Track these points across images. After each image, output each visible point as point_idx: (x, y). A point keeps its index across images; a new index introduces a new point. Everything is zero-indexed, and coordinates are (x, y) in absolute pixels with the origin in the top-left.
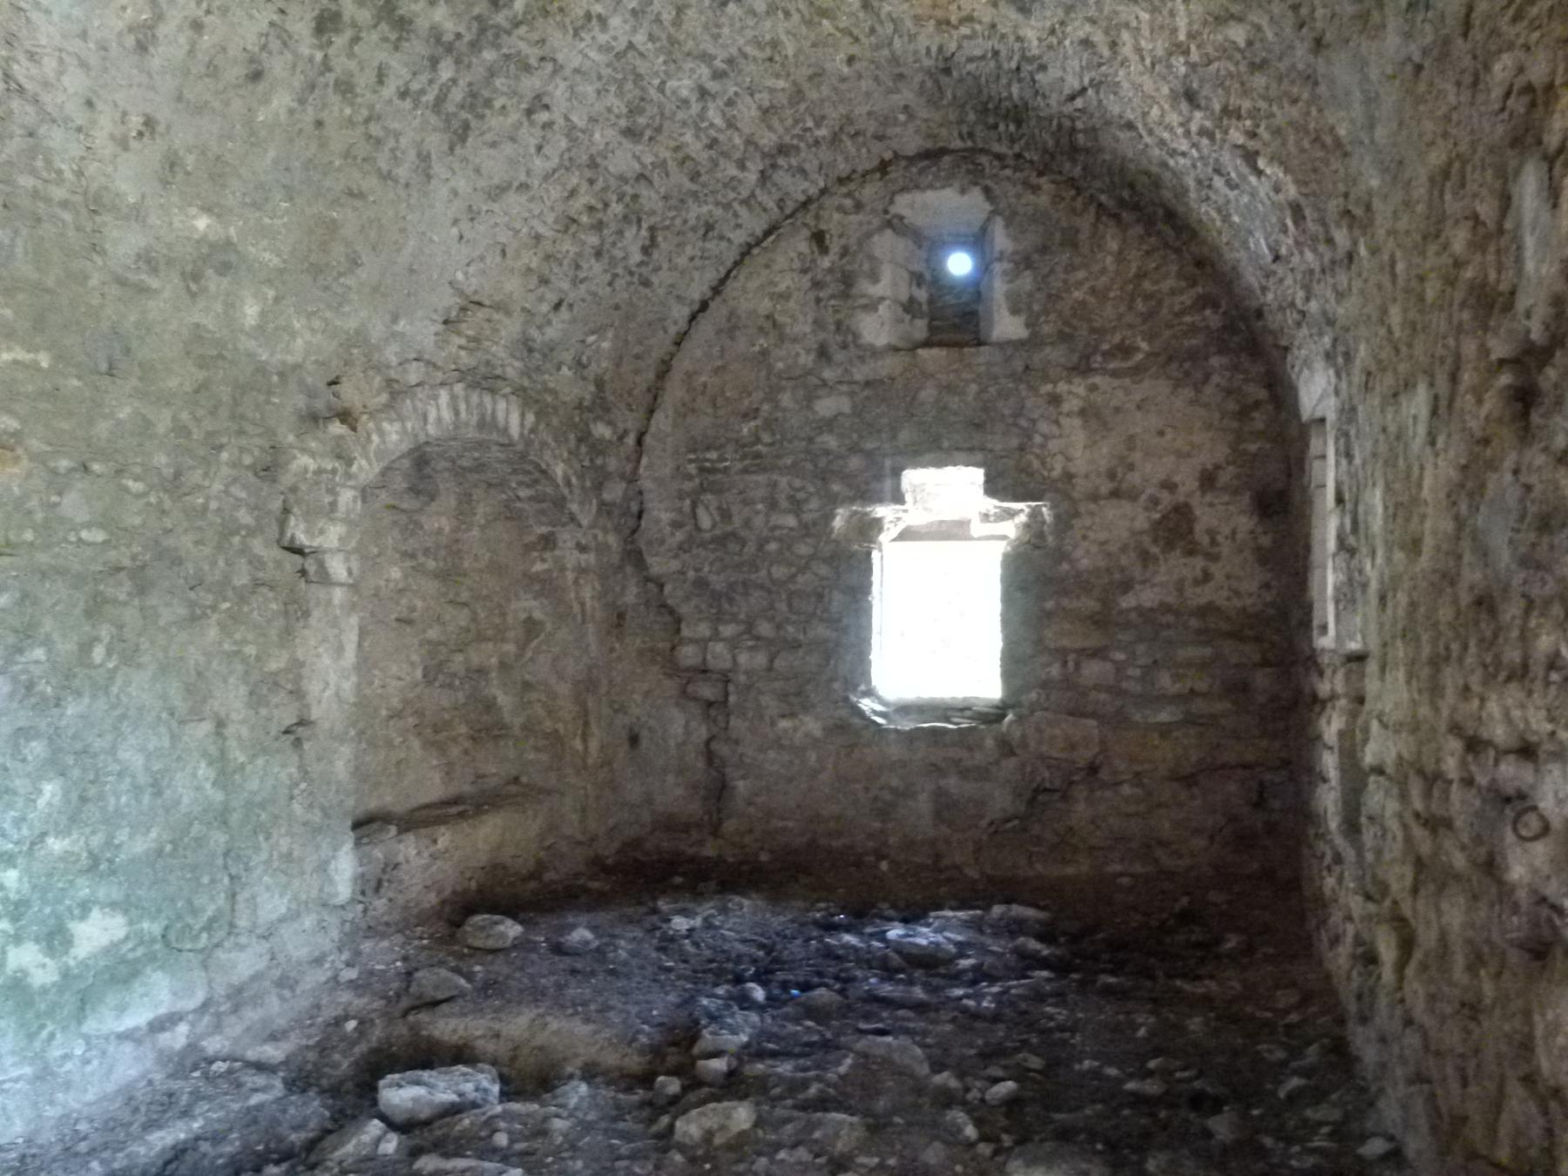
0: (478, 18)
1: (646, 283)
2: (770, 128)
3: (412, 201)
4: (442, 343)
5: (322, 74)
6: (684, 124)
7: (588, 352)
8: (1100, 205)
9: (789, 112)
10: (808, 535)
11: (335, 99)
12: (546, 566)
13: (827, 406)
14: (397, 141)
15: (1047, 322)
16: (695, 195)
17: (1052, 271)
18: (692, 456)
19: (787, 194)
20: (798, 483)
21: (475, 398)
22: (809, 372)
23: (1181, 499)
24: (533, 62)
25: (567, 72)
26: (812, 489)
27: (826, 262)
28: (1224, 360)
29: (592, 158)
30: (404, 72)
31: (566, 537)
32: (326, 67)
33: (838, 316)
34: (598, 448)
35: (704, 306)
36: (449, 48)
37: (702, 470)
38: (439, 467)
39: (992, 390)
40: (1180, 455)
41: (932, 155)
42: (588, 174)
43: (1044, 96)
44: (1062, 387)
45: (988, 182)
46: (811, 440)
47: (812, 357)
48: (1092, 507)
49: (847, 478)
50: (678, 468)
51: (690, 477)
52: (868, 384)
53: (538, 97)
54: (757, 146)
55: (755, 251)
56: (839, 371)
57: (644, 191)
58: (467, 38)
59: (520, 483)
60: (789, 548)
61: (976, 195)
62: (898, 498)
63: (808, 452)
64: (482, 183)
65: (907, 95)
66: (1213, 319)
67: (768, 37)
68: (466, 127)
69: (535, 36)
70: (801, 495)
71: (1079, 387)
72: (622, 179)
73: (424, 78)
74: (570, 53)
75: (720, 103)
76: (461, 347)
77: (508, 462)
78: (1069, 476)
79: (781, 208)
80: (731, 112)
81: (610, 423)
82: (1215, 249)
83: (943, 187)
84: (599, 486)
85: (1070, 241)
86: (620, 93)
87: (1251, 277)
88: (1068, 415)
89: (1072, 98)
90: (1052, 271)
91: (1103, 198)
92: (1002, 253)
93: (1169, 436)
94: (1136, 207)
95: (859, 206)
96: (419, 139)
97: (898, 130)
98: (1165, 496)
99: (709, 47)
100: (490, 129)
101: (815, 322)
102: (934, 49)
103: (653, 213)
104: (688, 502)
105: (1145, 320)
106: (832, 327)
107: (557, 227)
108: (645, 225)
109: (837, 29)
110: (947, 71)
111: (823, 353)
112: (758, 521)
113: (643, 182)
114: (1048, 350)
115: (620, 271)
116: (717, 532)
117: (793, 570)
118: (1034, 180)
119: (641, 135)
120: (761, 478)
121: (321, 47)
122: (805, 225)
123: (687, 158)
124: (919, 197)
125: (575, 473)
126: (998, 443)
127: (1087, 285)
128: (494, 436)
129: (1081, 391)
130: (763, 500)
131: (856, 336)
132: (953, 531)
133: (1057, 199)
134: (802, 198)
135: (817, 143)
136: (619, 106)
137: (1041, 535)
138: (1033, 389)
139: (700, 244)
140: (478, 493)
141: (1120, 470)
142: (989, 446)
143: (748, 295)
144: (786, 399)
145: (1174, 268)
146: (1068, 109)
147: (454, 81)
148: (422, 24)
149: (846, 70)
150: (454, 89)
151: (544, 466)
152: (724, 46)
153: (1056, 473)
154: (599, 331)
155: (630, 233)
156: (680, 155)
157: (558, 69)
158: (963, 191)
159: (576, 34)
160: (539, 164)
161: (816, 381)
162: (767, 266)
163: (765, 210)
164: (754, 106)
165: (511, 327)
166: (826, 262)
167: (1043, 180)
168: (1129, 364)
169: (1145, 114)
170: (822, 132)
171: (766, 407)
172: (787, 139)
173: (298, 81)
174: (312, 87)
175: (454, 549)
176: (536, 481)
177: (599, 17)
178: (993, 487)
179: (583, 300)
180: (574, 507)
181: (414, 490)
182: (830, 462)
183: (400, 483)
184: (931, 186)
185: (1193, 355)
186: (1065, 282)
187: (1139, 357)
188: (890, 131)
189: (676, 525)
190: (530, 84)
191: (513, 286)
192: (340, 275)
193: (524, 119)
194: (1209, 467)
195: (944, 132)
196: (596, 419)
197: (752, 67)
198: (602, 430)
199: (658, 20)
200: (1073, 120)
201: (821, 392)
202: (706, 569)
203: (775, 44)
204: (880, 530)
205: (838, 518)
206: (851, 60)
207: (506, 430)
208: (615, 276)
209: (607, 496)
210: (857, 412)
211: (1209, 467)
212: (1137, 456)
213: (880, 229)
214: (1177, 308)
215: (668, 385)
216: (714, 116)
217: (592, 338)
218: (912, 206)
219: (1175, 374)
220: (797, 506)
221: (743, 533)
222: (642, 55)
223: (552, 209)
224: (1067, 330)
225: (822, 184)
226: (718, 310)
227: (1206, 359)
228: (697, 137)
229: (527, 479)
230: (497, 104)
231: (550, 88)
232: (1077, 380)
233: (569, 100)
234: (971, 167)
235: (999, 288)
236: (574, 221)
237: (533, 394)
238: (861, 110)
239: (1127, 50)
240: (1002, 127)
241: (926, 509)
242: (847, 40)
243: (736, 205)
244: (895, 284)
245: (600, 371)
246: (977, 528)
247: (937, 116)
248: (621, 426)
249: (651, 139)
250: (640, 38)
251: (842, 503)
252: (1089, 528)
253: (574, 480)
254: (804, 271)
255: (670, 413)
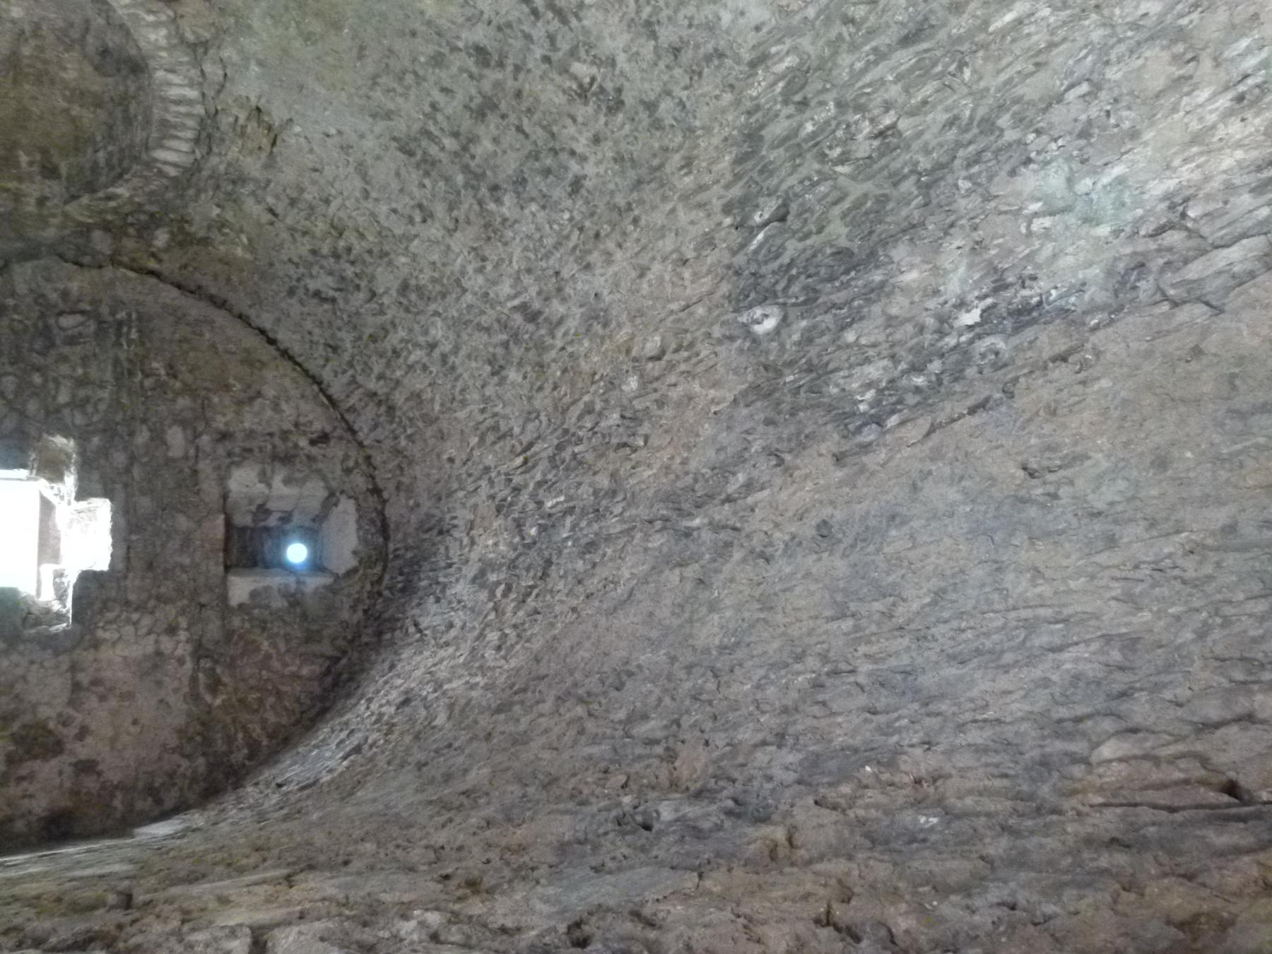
0: (484, 174)
1: (291, 292)
2: (407, 399)
3: (356, 99)
4: (242, 102)
5: (448, 43)
6: (411, 330)
7: (232, 235)
8: (339, 659)
9: (417, 414)
10: (48, 413)
11: (431, 49)
12: (24, 165)
13: (176, 438)
14: (401, 95)
15: (243, 620)
16: (360, 338)
17: (285, 623)
18: (134, 316)
19: (359, 415)
20: (102, 407)
21: (191, 123)
22: (207, 424)
23: (68, 746)
24: (455, 213)
25: (448, 240)
26: (95, 419)
27: (303, 443)
28: (202, 769)
29: (387, 254)
30: (449, 111)
31: (54, 188)
32: (455, 49)
33: (256, 450)
34: (145, 232)
35: (272, 342)
36: (465, 148)
37: (120, 324)
38: (129, 82)
39: (184, 577)
40: (113, 741)
41: (384, 529)
42: (376, 250)
43: (420, 604)
44: (183, 635)
45: (361, 572)
46: (144, 421)
47: (221, 426)
48: (65, 667)
49: (104, 452)
50: (123, 303)
51: (113, 313)
52: (195, 472)
53: (432, 216)
54: (394, 389)
55: (315, 387)
56: (208, 449)
57: (362, 296)
58: (473, 164)
59: (110, 154)
60: (35, 394)
61: (353, 563)
62: (82, 494)
63: (133, 418)
64: (369, 161)
65: (426, 504)
66: (239, 756)
67: (468, 397)
68: (411, 154)
69: (472, 217)
70: (90, 409)
71: (183, 650)
72: (372, 278)
73: (445, 125)
74: (460, 242)
75: (425, 360)
76: (237, 119)
77: (132, 146)
78: (96, 645)
79: (348, 410)
80: (418, 367)
81: (167, 249)
82: (296, 746)
83: (359, 537)
84: (106, 227)
85: (310, 638)
86: (434, 281)
87: (267, 774)
88: (157, 642)
89: (416, 625)
90: (285, 623)
91: (344, 661)
92: (304, 583)
93: (132, 729)
94: (335, 684)
95: (348, 471)
96: (403, 113)
97: (403, 501)
98: (73, 731)
99: (463, 353)
100: (409, 173)
101: (252, 431)
102: (455, 522)
103: (347, 302)
104: (88, 308)
105: (240, 701)
106: (247, 445)
107: (336, 220)
108: (337, 294)
109: (472, 449)
110: (441, 532)
111: (224, 436)
112: (64, 369)
113: (368, 295)
114: (218, 623)
115: (302, 270)
116: (55, 331)
117: (11, 397)
118: (361, 607)
119: (404, 296)
120: (108, 376)
121: (466, 47)
122: (335, 428)
123: (387, 332)
124: (352, 518)
125: (119, 207)
126: (133, 582)
127: (272, 651)
128: (155, 135)
129: (179, 652)
130: (85, 374)
131: (238, 464)
132: (48, 546)
133: (345, 625)
134: (356, 427)
135: (396, 438)
136: (424, 279)
137: (38, 622)
138: (183, 612)
139: (322, 341)
140: (102, 115)
141: (101, 689)
142: (131, 575)
143: (277, 379)
144: (184, 402)
145: (284, 721)
146: (409, 622)
147: (443, 149)
148: (481, 130)
149: (445, 457)
150: (436, 148)
151: (126, 177)
152: (463, 363)
153: (100, 634)
154: (251, 247)
155: (330, 280)
156: (389, 327)
157: (451, 232)
158: (355, 553)
159: (474, 249)
160: (383, 209)
161: (200, 429)
162: (303, 396)
163: (348, 396)
164: (422, 387)
165: (253, 166)
166: (303, 443)
167: (360, 614)
168: (202, 689)
169: (398, 676)
170: (403, 442)
171: (178, 385)
172: (398, 413)
173: (444, 23)
174: (439, 34)
175: (43, 78)
176: (111, 168)
177: (484, 267)
178: (88, 579)
179: (277, 235)
180: (85, 200)
181: (105, 52)
182: (122, 437)
183: (113, 40)
184: (360, 528)
185: (208, 742)
186: (277, 635)
187: (208, 698)
188: (402, 494)
189: (65, 294)
190: (439, 209)
191: (288, 175)
192: (298, 24)
193: (416, 202)
194: (100, 767)
195: (400, 536)
196: (172, 233)
197: (449, 386)
198: (161, 238)
199: (483, 313)
200: (401, 628)
201: (189, 432)
202: (16, 317)
203: (464, 403)
204: (51, 480)
205: (64, 441)
206: (451, 460)
207: (162, 147)
208: (297, 265)
209: (97, 235)
210: (169, 462)
211: (100, 767)
212: (113, 703)
213: (328, 487)
214: (250, 726)
215: (202, 304)
216: (417, 355)
217: (245, 240)
218: (345, 512)
219: (191, 730)
220: (79, 404)
221: (53, 352)
222: (458, 299)
223: (350, 217)
224: (235, 637)
225: (366, 443)
226: (266, 352)
227: (204, 754)
228: (402, 341)
229: (115, 161)
230: (427, 182)
231: (437, 225)
232: (189, 648)
233: (429, 240)
234: (374, 558)
235: (275, 581)
236: (341, 234)
237: (194, 179)
238: (418, 471)
239: (442, 653)
240: (400, 578)
241: (72, 521)
242: (464, 457)
243: (351, 372)
244: (281, 497)
245: (216, 244)
246: (48, 570)
247: (411, 530)
248: (165, 257)
249: (401, 303)
250: (469, 298)
251: (78, 444)
252: (42, 666)
253: (112, 204)
254: (296, 425)
255: (176, 302)
